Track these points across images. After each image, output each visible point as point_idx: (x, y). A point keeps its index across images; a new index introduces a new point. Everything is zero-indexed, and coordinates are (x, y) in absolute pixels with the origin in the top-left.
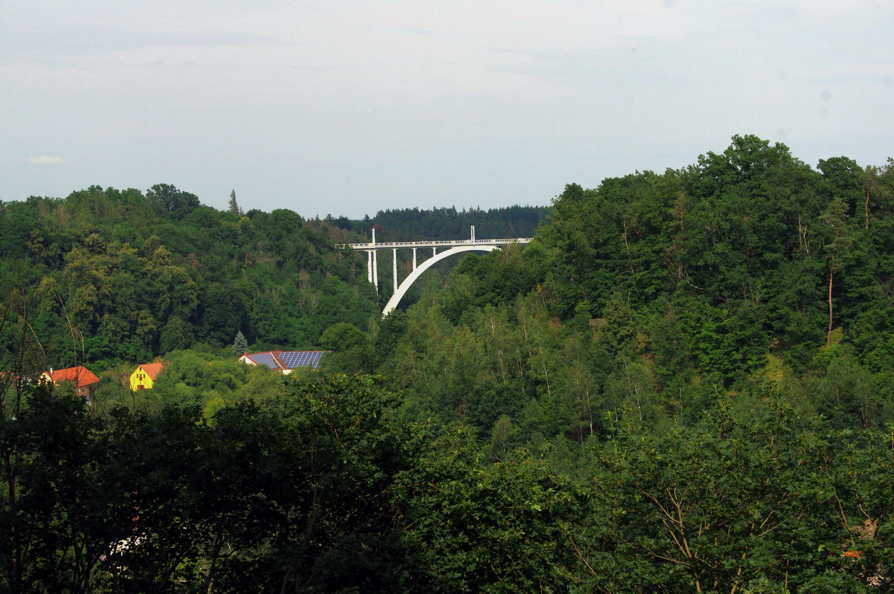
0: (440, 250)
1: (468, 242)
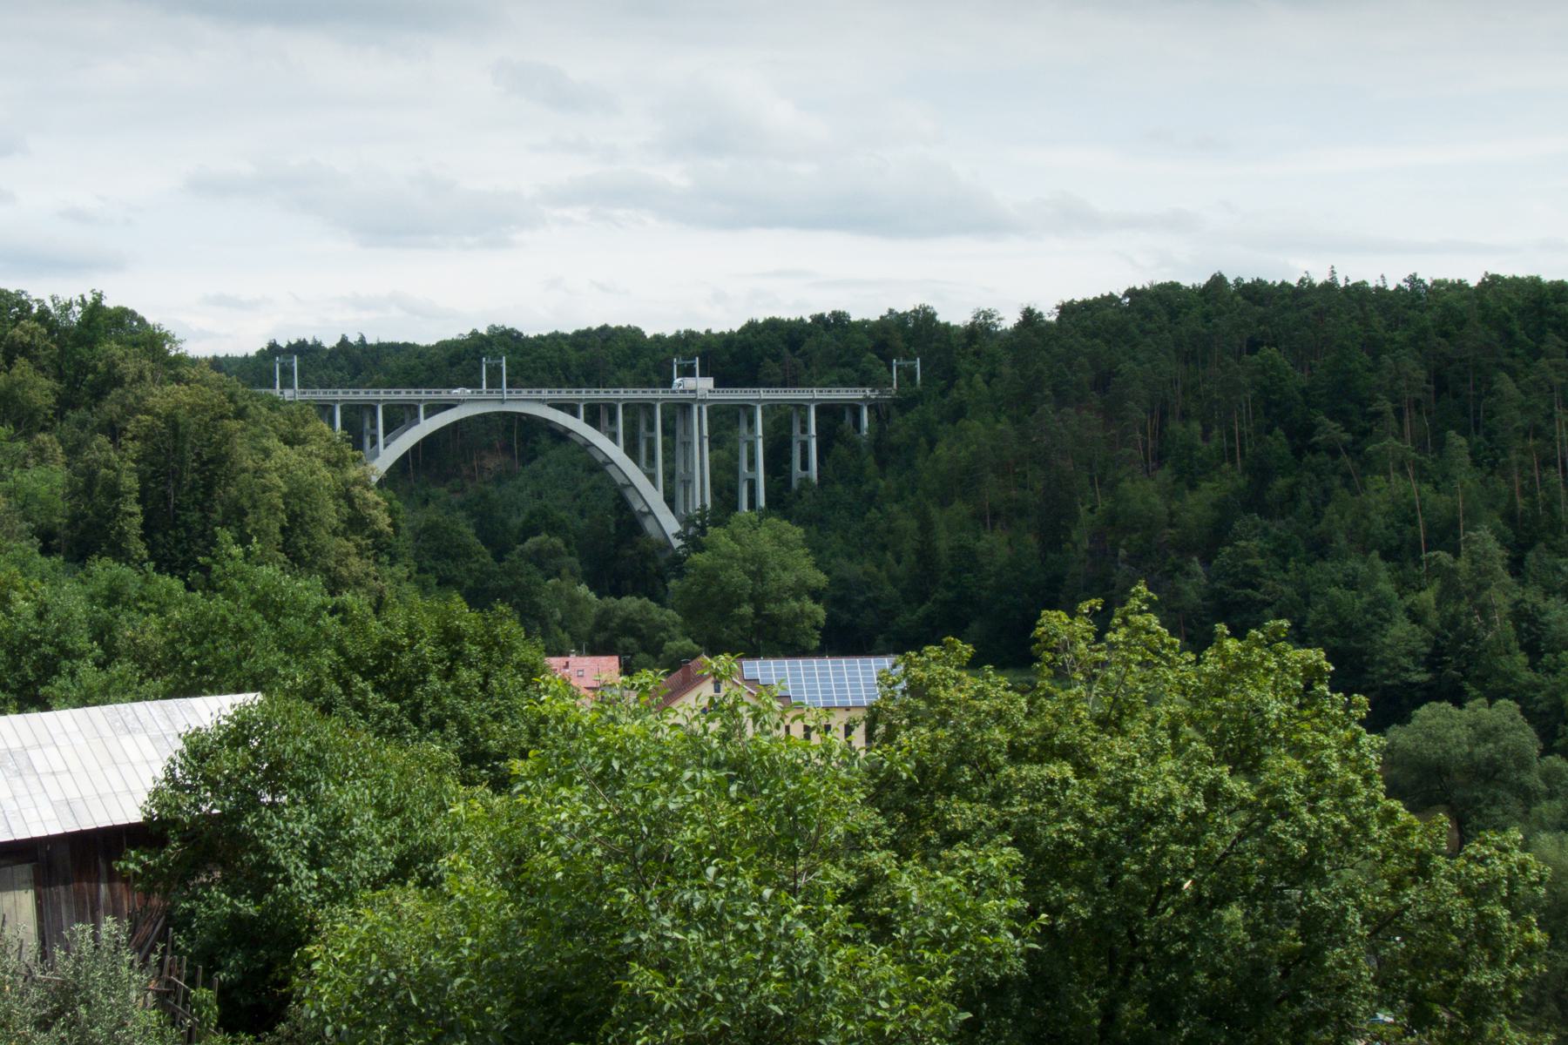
0: (434, 409)
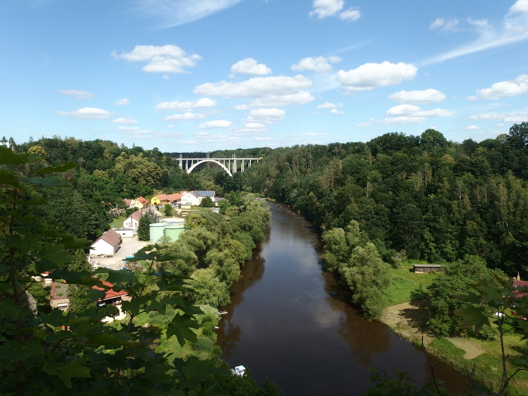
0: (199, 161)
1: (206, 159)
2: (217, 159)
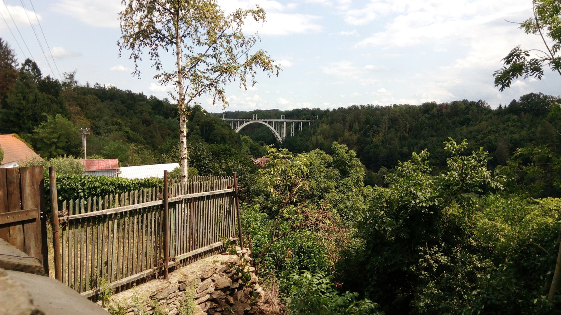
0: (246, 122)
2: (265, 120)
